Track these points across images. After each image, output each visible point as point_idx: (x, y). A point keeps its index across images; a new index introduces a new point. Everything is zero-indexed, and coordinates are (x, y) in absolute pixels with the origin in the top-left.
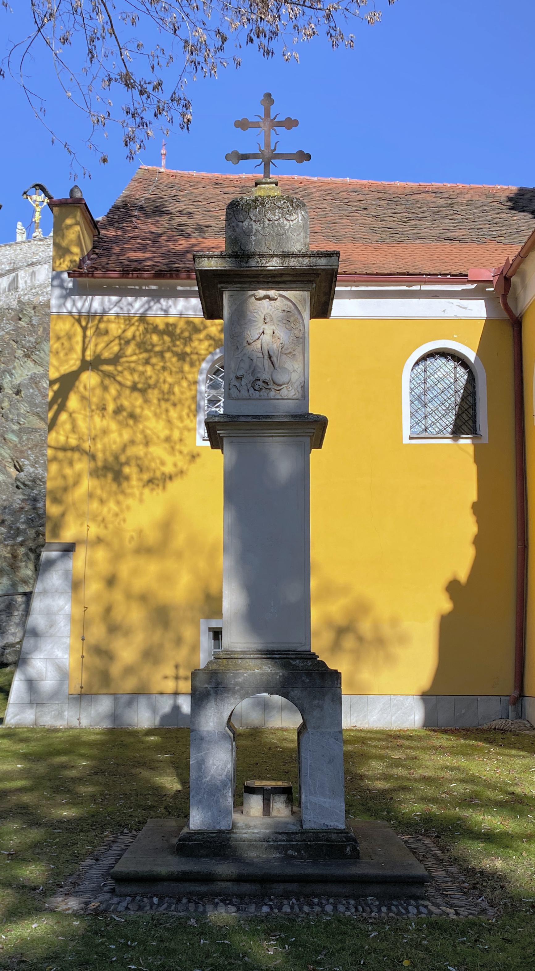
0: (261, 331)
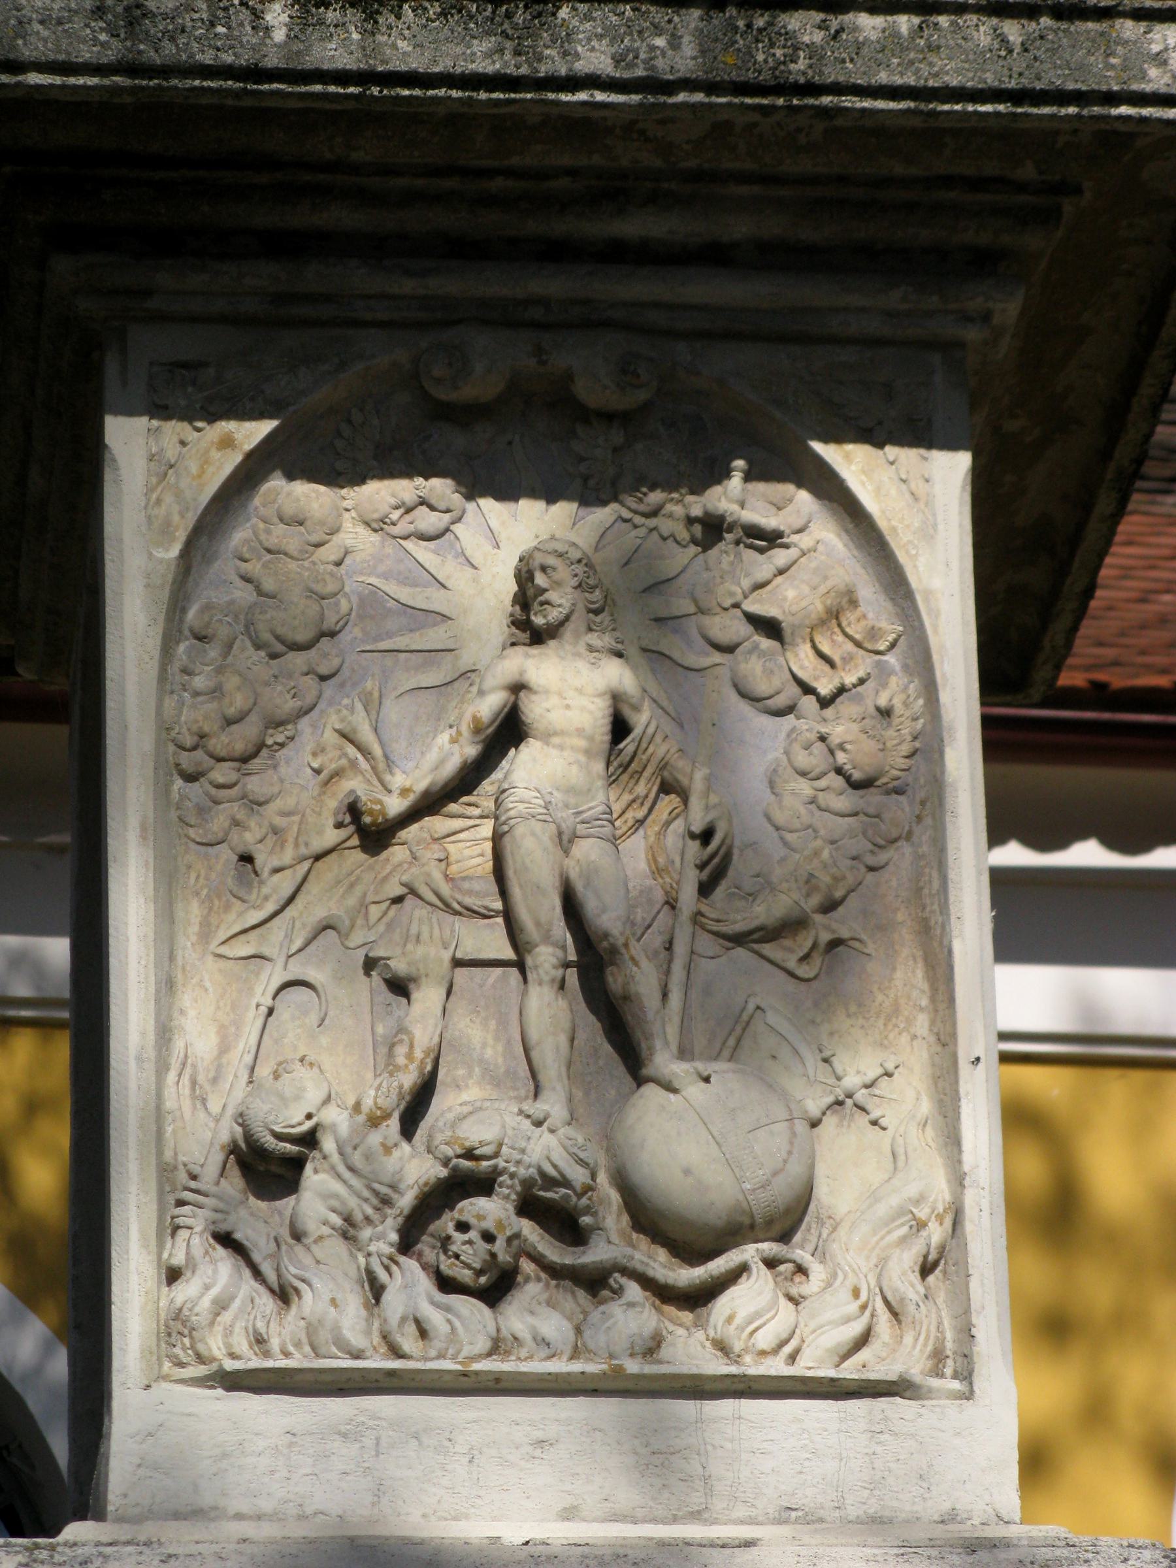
0: (489, 705)
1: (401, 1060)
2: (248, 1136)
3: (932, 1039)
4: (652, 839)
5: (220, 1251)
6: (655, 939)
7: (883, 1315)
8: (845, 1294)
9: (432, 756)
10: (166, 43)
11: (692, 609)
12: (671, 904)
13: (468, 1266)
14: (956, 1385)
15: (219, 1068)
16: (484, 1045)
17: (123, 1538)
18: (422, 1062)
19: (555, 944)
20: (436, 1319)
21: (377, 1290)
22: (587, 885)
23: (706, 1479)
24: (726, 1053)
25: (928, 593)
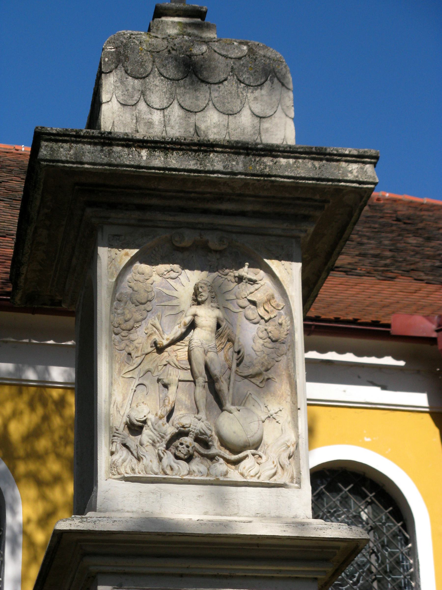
0: (188, 319)
1: (167, 404)
2: (130, 420)
3: (291, 402)
4: (225, 353)
5: (124, 448)
6: (226, 376)
7: (280, 468)
8: (271, 463)
9: (174, 331)
10: (118, 159)
11: (235, 298)
12: (230, 368)
13: (183, 453)
14: (297, 485)
15: (123, 404)
16: (186, 400)
17: (103, 516)
18: (172, 404)
19: (203, 377)
20: (175, 466)
21: (160, 459)
22: (211, 363)
23: (238, 506)
24: (242, 404)
25: (291, 296)
